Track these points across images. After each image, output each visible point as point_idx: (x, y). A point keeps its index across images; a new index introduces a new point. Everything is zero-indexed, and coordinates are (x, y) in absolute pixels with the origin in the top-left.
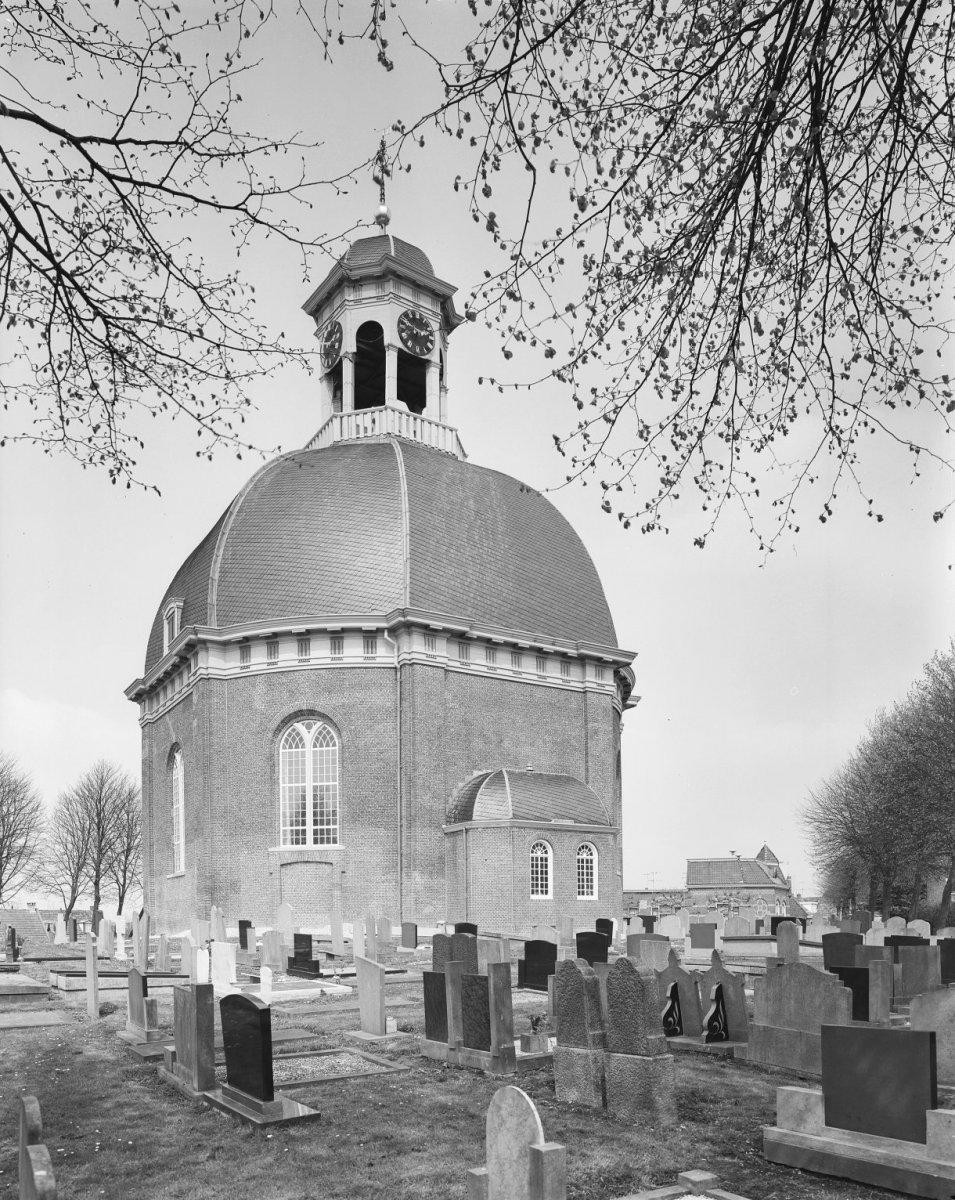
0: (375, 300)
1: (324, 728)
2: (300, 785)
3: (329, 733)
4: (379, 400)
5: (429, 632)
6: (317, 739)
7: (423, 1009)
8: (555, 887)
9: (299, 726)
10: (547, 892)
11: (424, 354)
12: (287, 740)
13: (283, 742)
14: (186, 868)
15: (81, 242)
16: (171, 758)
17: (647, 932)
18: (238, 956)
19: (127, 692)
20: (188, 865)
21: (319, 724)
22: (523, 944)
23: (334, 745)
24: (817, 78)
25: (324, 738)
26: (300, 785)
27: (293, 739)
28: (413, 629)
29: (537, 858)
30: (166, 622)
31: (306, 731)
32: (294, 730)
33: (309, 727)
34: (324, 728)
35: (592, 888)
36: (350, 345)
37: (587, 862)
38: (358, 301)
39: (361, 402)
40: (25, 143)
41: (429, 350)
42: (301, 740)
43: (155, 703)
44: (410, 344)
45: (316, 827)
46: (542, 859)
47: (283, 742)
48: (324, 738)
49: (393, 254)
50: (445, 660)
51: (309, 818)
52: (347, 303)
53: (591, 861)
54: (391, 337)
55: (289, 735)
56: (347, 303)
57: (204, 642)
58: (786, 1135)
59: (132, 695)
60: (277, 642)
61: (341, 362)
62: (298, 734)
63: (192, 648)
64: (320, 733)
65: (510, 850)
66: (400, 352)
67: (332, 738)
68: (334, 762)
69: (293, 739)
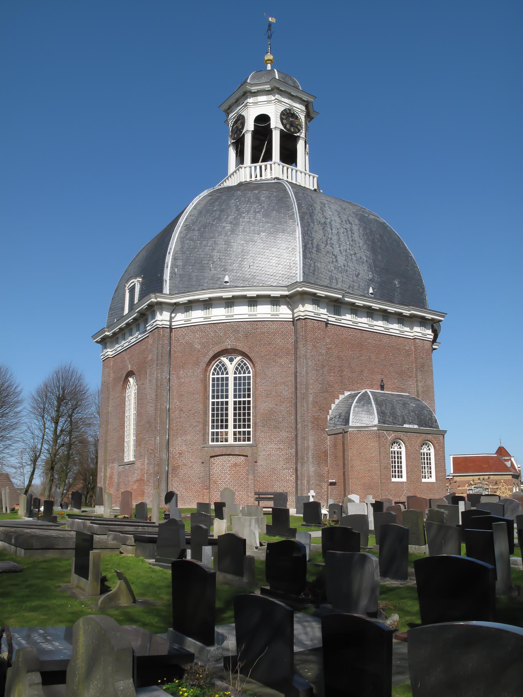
0: (266, 102)
3: (245, 364)
4: (268, 157)
5: (316, 300)
6: (237, 369)
8: (407, 473)
9: (225, 360)
10: (401, 477)
11: (297, 133)
12: (215, 369)
13: (212, 370)
14: (135, 456)
16: (126, 381)
19: (94, 337)
20: (138, 454)
21: (240, 357)
22: (366, 514)
23: (249, 373)
25: (242, 368)
27: (220, 368)
28: (305, 296)
29: (394, 452)
30: (127, 291)
31: (229, 363)
33: (231, 360)
34: (242, 361)
35: (401, 472)
36: (250, 126)
37: (398, 454)
38: (255, 103)
39: (255, 160)
41: (299, 131)
42: (226, 369)
44: (288, 126)
46: (398, 452)
47: (212, 370)
48: (242, 368)
49: (277, 78)
50: (326, 317)
52: (248, 104)
53: (430, 454)
54: (275, 123)
55: (217, 366)
56: (248, 104)
57: (160, 304)
58: (82, 622)
59: (98, 339)
60: (340, 306)
61: (244, 135)
62: (223, 365)
63: (153, 309)
64: (239, 365)
65: (377, 444)
66: (281, 131)
67: (247, 368)
69: (220, 368)
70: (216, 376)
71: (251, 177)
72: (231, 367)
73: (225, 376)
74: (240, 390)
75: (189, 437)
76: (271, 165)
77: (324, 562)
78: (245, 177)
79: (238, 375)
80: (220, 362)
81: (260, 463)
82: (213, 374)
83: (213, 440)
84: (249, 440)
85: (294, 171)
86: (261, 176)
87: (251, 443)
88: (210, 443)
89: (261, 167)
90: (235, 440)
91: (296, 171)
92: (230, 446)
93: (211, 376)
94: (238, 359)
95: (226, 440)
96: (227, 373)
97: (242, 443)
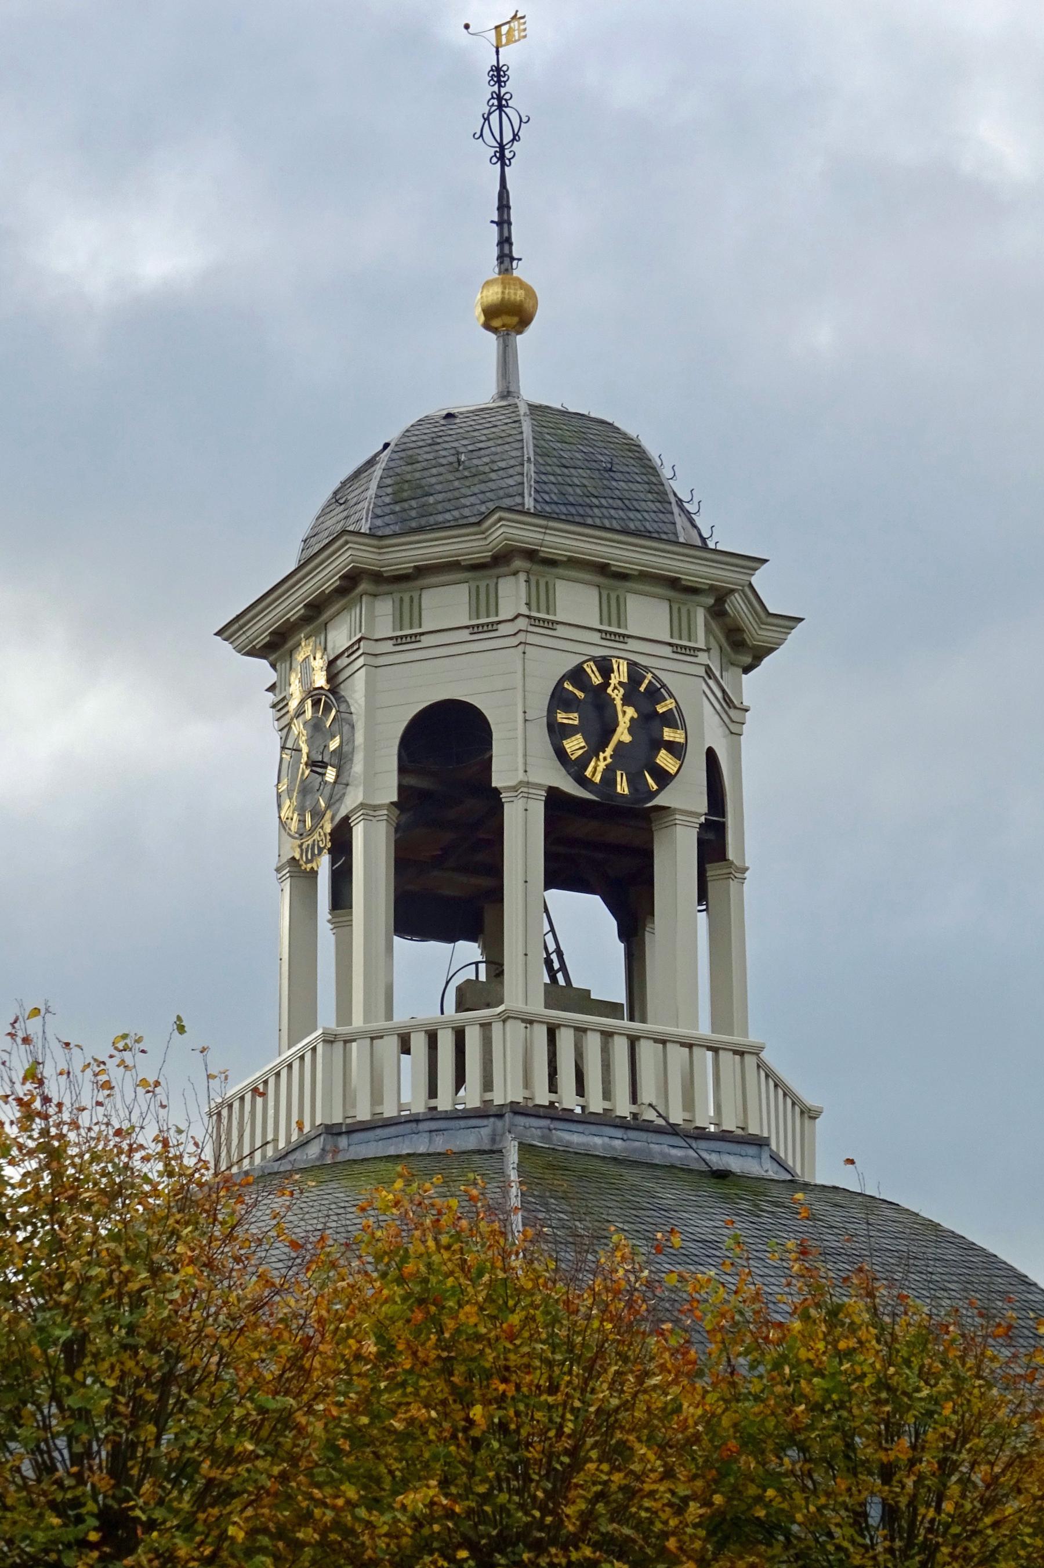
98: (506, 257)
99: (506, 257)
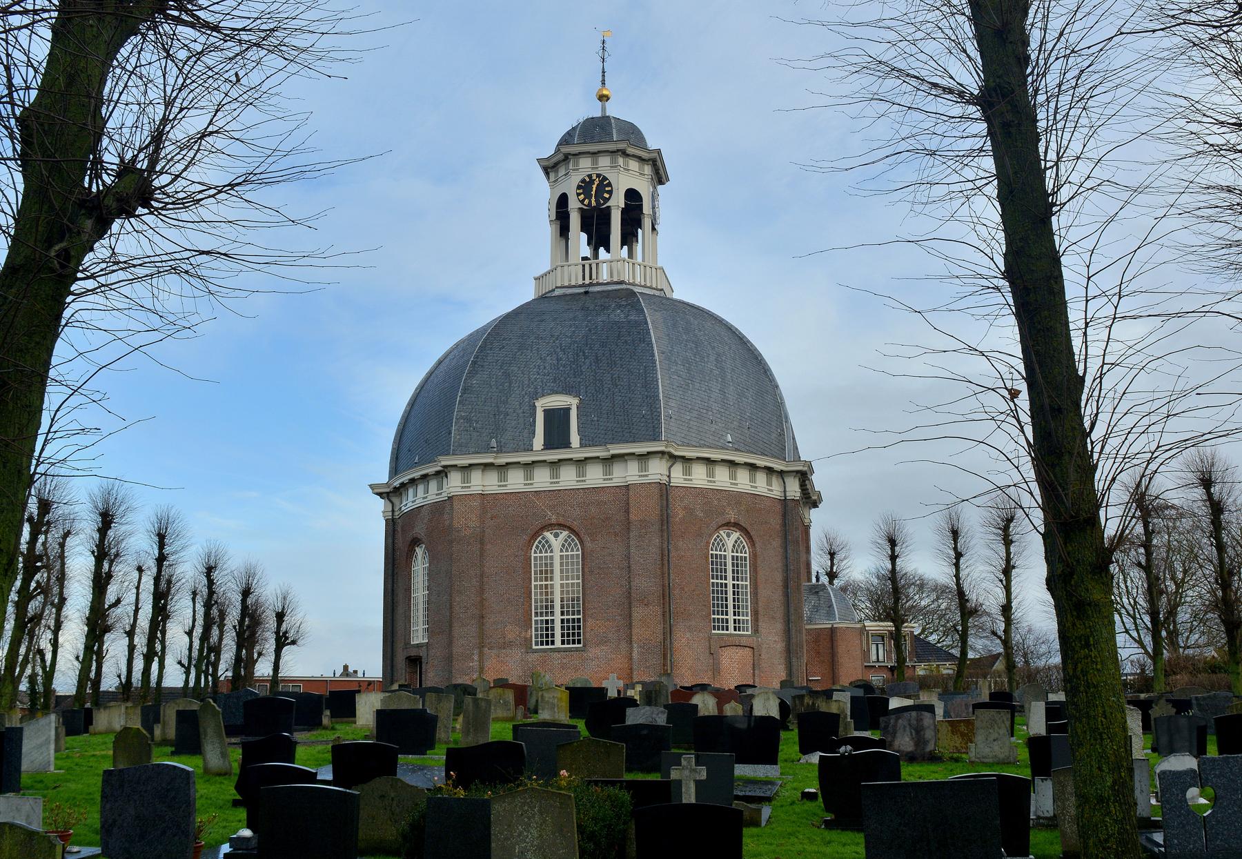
1: (569, 537)
2: (565, 582)
3: (742, 542)
6: (563, 545)
7: (1031, 842)
9: (548, 535)
12: (537, 547)
15: (132, 73)
17: (1176, 713)
18: (364, 692)
23: (745, 553)
24: (31, 533)
25: (569, 545)
26: (565, 582)
27: (543, 546)
32: (543, 538)
33: (556, 536)
40: (2, 184)
42: (550, 546)
43: (404, 498)
45: (563, 617)
48: (569, 545)
51: (557, 610)
55: (540, 542)
62: (547, 542)
64: (566, 541)
68: (578, 564)
69: (543, 546)
70: (538, 555)
71: (584, 279)
72: (730, 543)
73: (549, 554)
74: (567, 571)
75: (693, 623)
76: (597, 264)
77: (236, 803)
78: (576, 280)
79: (565, 553)
80: (718, 537)
81: (763, 657)
82: (535, 552)
83: (537, 644)
84: (579, 642)
85: (631, 264)
86: (591, 278)
87: (581, 645)
88: (534, 647)
89: (590, 265)
90: (563, 642)
91: (633, 264)
92: (731, 635)
93: (533, 555)
94: (736, 535)
95: (553, 643)
96: (551, 551)
97: (571, 646)
98: (603, 83)
99: (603, 83)
